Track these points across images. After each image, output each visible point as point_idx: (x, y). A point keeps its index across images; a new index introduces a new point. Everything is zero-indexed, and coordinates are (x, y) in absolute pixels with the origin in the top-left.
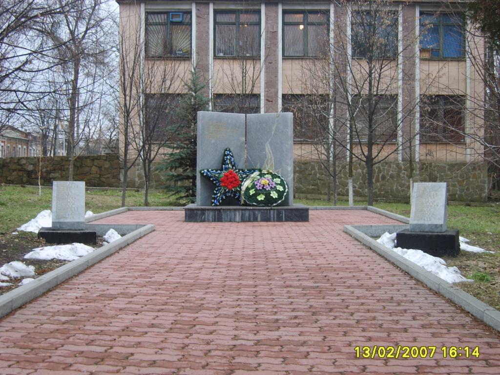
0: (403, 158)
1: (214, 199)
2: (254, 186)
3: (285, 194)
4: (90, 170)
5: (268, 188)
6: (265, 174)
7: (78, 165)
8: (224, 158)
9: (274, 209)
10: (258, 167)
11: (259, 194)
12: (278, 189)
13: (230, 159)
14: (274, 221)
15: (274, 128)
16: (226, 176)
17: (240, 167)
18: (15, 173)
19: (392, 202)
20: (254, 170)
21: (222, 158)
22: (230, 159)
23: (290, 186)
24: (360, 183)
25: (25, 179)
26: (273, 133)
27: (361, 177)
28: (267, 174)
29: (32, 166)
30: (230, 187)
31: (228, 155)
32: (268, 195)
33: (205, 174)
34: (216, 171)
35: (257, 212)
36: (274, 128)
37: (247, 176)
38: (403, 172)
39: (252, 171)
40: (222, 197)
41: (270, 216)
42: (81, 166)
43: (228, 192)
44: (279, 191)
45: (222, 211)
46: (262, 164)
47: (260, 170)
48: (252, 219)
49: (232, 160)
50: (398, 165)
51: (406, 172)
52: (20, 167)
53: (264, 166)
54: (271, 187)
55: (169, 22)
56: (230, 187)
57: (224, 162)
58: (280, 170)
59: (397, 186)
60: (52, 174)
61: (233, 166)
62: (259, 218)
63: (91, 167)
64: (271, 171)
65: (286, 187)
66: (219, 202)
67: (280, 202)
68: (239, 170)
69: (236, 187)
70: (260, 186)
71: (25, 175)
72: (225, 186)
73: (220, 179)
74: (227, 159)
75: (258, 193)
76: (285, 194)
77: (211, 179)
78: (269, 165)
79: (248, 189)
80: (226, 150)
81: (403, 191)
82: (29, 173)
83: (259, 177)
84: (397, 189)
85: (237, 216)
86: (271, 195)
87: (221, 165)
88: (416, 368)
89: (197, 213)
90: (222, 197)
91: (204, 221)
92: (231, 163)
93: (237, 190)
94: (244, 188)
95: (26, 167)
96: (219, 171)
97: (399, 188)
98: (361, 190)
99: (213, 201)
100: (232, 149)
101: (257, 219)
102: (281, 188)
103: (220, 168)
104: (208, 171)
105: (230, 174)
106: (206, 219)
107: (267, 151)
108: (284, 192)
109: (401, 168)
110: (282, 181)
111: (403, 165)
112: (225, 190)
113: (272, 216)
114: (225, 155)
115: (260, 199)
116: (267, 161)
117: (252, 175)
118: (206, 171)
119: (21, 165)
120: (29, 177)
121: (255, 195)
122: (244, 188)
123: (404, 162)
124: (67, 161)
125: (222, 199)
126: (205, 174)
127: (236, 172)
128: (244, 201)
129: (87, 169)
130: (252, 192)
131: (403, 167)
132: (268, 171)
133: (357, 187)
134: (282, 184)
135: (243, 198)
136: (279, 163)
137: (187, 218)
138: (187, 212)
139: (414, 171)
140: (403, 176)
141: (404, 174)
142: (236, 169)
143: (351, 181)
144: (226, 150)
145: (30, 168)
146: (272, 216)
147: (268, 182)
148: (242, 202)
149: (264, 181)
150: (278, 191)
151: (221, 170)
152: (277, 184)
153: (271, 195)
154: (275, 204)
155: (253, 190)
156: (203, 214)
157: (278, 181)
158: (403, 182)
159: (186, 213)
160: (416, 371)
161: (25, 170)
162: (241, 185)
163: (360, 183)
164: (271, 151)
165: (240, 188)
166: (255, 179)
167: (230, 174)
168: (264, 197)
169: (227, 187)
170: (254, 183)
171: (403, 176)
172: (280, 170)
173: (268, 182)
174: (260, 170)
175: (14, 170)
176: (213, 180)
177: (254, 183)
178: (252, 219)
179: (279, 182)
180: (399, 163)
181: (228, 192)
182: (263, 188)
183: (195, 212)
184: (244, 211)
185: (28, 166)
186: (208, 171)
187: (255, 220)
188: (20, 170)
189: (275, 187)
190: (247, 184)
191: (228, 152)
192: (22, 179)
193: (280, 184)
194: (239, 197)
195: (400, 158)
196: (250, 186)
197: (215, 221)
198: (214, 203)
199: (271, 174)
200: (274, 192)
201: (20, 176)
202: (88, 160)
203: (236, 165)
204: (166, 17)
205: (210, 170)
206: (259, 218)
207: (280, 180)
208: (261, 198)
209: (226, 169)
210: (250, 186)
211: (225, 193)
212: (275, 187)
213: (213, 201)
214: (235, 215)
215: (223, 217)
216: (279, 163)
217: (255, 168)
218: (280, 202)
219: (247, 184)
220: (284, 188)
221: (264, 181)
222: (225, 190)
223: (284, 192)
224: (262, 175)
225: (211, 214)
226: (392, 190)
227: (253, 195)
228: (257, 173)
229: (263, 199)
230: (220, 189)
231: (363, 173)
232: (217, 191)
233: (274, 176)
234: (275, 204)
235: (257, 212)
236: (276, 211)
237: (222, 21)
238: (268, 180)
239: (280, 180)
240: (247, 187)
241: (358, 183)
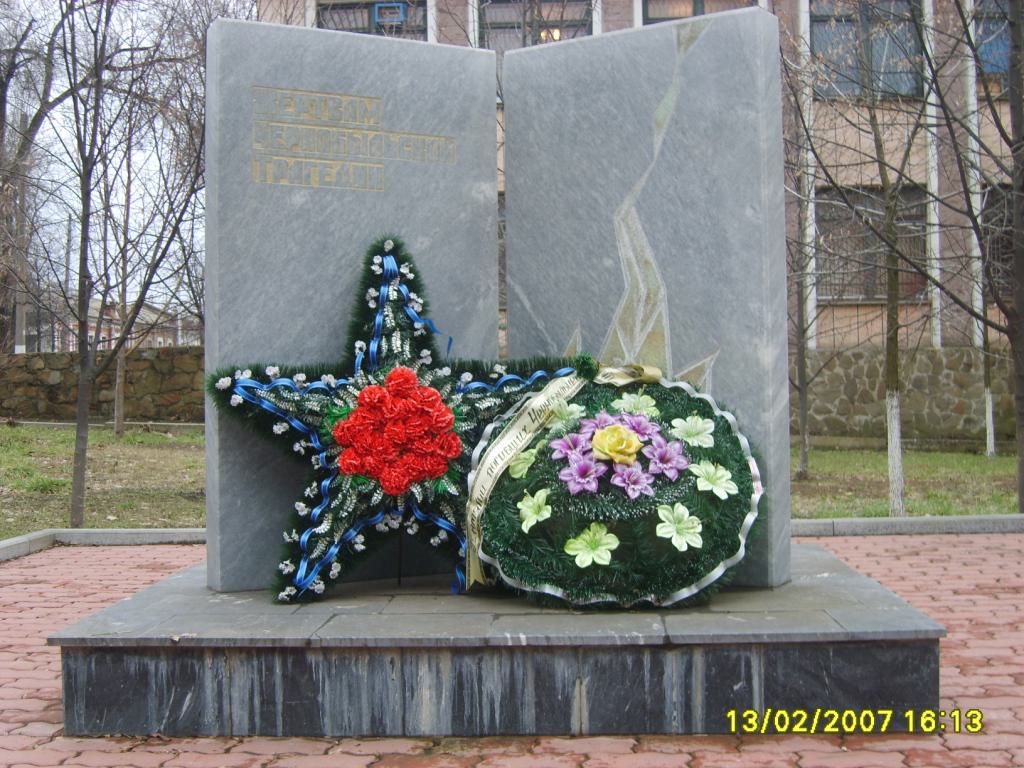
0: (943, 338)
1: (296, 553)
2: (544, 471)
3: (750, 518)
4: (192, 381)
5: (641, 486)
6: (618, 392)
7: (165, 371)
8: (362, 301)
9: (687, 648)
10: (575, 347)
11: (583, 525)
12: (702, 485)
13: (401, 304)
14: (688, 732)
15: (664, 111)
16: (371, 407)
17: (466, 352)
18: (19, 391)
19: (935, 451)
20: (551, 369)
21: (351, 301)
22: (401, 304)
23: (771, 464)
24: (842, 401)
25: (42, 405)
26: (658, 141)
27: (842, 388)
28: (632, 388)
29: (58, 373)
30: (394, 475)
31: (386, 278)
32: (637, 534)
33: (237, 399)
34: (313, 376)
35: (562, 668)
36: (664, 111)
37: (508, 403)
38: (946, 371)
39: (535, 371)
40: (346, 545)
41: (660, 698)
42: (171, 373)
43: (387, 507)
44: (710, 496)
45: (312, 658)
46: (596, 333)
47: (586, 369)
48: (528, 716)
49: (415, 308)
50: (932, 356)
51: (952, 373)
52: (30, 377)
53: (605, 350)
54: (660, 476)
55: (373, 26)
56: (394, 475)
57: (363, 323)
58: (709, 362)
59: (930, 408)
60: (104, 392)
61: (421, 343)
62: (580, 713)
63: (195, 373)
64: (651, 372)
65: (754, 469)
66: (324, 575)
67: (718, 572)
68: (458, 370)
69: (434, 476)
70: (584, 472)
71: (42, 396)
72: (360, 472)
73: (329, 426)
74: (381, 301)
75: (568, 519)
76: (750, 518)
77: (279, 429)
78: (640, 338)
79: (508, 489)
80: (379, 250)
81: (946, 418)
82: (52, 391)
83: (577, 410)
84: (931, 415)
85: (426, 694)
86: (661, 531)
87: (344, 339)
88: (902, 757)
89: (144, 674)
90: (346, 545)
91: (192, 729)
92: (406, 327)
93: (445, 497)
94: (481, 482)
95: (43, 377)
96: (329, 379)
97: (937, 411)
98: (843, 419)
99: (287, 567)
100: (415, 246)
101: (567, 715)
102: (719, 482)
103: (338, 358)
104: (259, 374)
105: (399, 394)
106: (210, 716)
107: (626, 252)
108: (738, 504)
109: (941, 363)
110: (723, 430)
111: (946, 355)
112: (365, 497)
113: (674, 695)
114: (373, 280)
115: (583, 560)
116: (630, 310)
117: (538, 401)
118: (245, 377)
119: (33, 372)
120: (51, 399)
121: (552, 534)
122: (481, 482)
123: (948, 349)
124: (137, 360)
125: (347, 554)
126: (237, 399)
127: (437, 384)
128: (487, 569)
129: (184, 379)
130: (533, 511)
131: (944, 361)
132: (635, 371)
133: (835, 410)
134: (725, 452)
135: (474, 549)
136: (699, 319)
137: (80, 706)
138: (82, 668)
139: (973, 370)
140: (945, 381)
141: (947, 376)
142: (437, 363)
143: (895, 402)
144: (379, 250)
145: (55, 378)
146: (674, 695)
147: (636, 441)
148: (474, 575)
149: (611, 438)
150: (704, 504)
151: (345, 370)
152: (695, 454)
153: (661, 531)
154: (685, 593)
155: (542, 494)
156: (187, 679)
157: (697, 431)
158: (946, 396)
159: (69, 675)
160: (904, 762)
161: (42, 384)
162: (466, 463)
163: (842, 401)
164: (649, 254)
165: (461, 481)
166: (557, 426)
167: (399, 394)
168: (613, 542)
169: (373, 474)
170: (545, 453)
171: (945, 381)
172: (709, 362)
173: (636, 441)
174: (586, 369)
175: (17, 385)
176: (292, 435)
177: (545, 453)
178: (528, 716)
179: (708, 442)
180: (934, 352)
181: (387, 507)
182: (604, 481)
183: (132, 664)
184: (469, 663)
185: (48, 374)
186: (259, 374)
187: (554, 721)
188: (31, 385)
189: (683, 473)
190: (504, 452)
191: (390, 263)
192: (35, 406)
193: (716, 456)
194: (457, 535)
195: (937, 340)
196: (520, 472)
197: (268, 730)
198: (289, 579)
199: (652, 387)
200: (681, 509)
201: (31, 398)
202: (187, 356)
203: (440, 341)
204: (366, 16)
205: (271, 371)
206: (580, 713)
207: (710, 425)
208: (593, 549)
209: (372, 363)
210: (520, 472)
211: (363, 519)
212: (683, 473)
213: (287, 567)
214: (408, 688)
215: (326, 698)
216: (699, 319)
217: (554, 352)
218: (718, 572)
219: (504, 452)
220: (741, 475)
221: (611, 438)
222: (365, 497)
223: (738, 504)
224: (596, 397)
225: (242, 679)
226: (919, 417)
227: (539, 527)
228: (566, 385)
229: (604, 559)
230: (334, 492)
231: (847, 375)
232: (311, 503)
233: (674, 404)
234: (685, 593)
235: (562, 668)
236: (699, 659)
237: (500, 19)
238: (637, 429)
239: (710, 425)
240: (506, 474)
241: (837, 402)
